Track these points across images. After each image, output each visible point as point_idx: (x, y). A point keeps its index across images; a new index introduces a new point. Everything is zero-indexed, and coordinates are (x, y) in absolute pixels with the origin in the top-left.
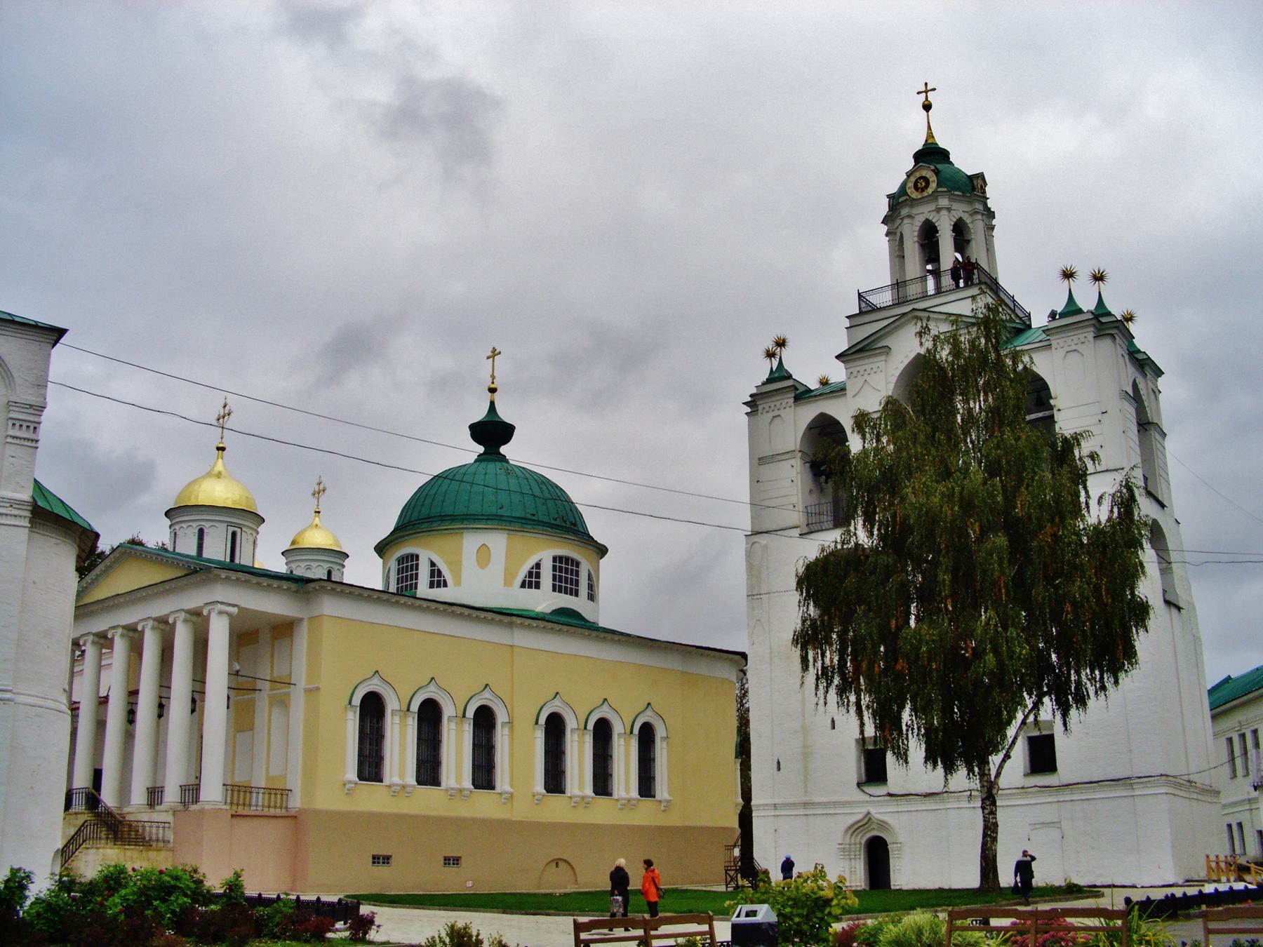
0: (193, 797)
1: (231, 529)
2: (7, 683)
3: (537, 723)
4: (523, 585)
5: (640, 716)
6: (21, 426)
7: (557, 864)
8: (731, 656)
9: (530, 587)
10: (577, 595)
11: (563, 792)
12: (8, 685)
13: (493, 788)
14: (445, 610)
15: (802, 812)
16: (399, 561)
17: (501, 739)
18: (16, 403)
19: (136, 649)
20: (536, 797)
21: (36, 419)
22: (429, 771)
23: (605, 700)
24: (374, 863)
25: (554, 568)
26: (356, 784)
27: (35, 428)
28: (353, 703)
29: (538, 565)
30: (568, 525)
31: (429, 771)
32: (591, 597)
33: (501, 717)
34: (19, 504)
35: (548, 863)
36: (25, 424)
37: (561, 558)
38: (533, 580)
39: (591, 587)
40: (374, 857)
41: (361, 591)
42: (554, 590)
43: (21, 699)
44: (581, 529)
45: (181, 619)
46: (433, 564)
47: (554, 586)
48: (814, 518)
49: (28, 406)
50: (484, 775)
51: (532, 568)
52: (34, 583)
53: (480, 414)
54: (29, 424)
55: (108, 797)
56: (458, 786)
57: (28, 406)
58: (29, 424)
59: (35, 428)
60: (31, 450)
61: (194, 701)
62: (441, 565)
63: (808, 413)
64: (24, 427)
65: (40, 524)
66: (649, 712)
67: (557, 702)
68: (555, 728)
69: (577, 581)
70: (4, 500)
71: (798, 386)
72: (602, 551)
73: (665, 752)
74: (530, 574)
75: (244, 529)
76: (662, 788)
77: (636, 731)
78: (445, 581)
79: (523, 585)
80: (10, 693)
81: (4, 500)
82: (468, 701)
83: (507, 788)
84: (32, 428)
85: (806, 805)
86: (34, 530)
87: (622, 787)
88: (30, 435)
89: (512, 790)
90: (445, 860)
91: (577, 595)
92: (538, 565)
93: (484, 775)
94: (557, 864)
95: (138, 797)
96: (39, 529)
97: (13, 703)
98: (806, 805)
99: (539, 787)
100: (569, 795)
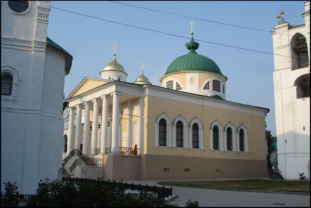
0: (20, 46)
1: (118, 77)
2: (38, 108)
3: (211, 128)
4: (204, 89)
5: (240, 127)
6: (41, 16)
7: (217, 171)
8: (265, 110)
9: (206, 89)
10: (220, 92)
11: (219, 149)
12: (39, 109)
13: (198, 148)
14: (183, 94)
15: (294, 155)
16: (167, 83)
17: (201, 132)
18: (39, 7)
19: (91, 108)
20: (211, 151)
21: (47, 13)
22: (180, 142)
23: (230, 122)
24: (164, 170)
25: (213, 83)
26: (158, 146)
27: (47, 17)
28: (157, 122)
29: (208, 83)
30: (216, 71)
31: (180, 142)
32: (224, 92)
33: (200, 126)
34: (41, 43)
35: (215, 171)
36: (43, 15)
37: (215, 80)
38: (207, 87)
39: (223, 89)
40: (164, 169)
41: (159, 88)
42: (213, 90)
43: (44, 114)
44: (220, 72)
45: (104, 98)
46: (177, 83)
47: (213, 89)
48: (295, 65)
49: (44, 9)
50: (196, 145)
51: (207, 83)
52: (48, 72)
53: (189, 41)
54: (44, 15)
55: (84, 152)
56: (188, 147)
57: (44, 9)
58: (44, 15)
59: (47, 17)
60: (46, 24)
61: (109, 123)
62: (180, 83)
63: (293, 32)
64: (43, 16)
65: (50, 51)
66: (242, 126)
67: (216, 122)
68: (216, 130)
69: (220, 87)
70: (36, 42)
71: (289, 25)
72: (226, 79)
73: (247, 137)
74: (206, 85)
75: (122, 77)
76: (246, 149)
77: (239, 131)
78: (181, 88)
79: (204, 89)
80: (40, 112)
81: (36, 42)
82: (191, 122)
83: (202, 148)
84: (45, 17)
85: (295, 153)
86: (47, 53)
87: (235, 148)
88: (45, 19)
89: (204, 149)
90: (185, 170)
91: (220, 92)
92: (208, 83)
93: (196, 145)
94: (217, 171)
95: (93, 152)
96: (50, 53)
97: (41, 115)
98: (295, 153)
99: (212, 148)
100: (220, 150)
